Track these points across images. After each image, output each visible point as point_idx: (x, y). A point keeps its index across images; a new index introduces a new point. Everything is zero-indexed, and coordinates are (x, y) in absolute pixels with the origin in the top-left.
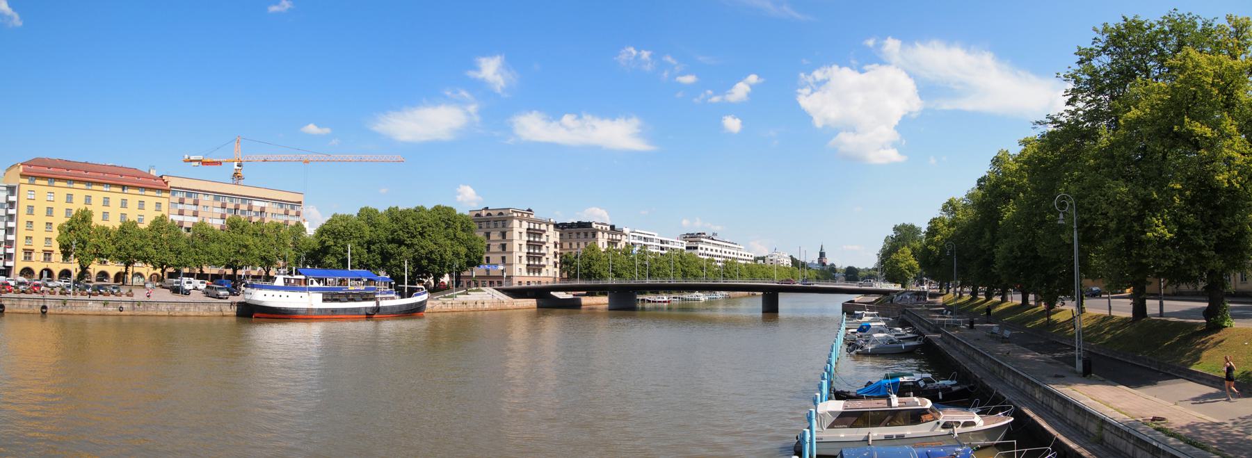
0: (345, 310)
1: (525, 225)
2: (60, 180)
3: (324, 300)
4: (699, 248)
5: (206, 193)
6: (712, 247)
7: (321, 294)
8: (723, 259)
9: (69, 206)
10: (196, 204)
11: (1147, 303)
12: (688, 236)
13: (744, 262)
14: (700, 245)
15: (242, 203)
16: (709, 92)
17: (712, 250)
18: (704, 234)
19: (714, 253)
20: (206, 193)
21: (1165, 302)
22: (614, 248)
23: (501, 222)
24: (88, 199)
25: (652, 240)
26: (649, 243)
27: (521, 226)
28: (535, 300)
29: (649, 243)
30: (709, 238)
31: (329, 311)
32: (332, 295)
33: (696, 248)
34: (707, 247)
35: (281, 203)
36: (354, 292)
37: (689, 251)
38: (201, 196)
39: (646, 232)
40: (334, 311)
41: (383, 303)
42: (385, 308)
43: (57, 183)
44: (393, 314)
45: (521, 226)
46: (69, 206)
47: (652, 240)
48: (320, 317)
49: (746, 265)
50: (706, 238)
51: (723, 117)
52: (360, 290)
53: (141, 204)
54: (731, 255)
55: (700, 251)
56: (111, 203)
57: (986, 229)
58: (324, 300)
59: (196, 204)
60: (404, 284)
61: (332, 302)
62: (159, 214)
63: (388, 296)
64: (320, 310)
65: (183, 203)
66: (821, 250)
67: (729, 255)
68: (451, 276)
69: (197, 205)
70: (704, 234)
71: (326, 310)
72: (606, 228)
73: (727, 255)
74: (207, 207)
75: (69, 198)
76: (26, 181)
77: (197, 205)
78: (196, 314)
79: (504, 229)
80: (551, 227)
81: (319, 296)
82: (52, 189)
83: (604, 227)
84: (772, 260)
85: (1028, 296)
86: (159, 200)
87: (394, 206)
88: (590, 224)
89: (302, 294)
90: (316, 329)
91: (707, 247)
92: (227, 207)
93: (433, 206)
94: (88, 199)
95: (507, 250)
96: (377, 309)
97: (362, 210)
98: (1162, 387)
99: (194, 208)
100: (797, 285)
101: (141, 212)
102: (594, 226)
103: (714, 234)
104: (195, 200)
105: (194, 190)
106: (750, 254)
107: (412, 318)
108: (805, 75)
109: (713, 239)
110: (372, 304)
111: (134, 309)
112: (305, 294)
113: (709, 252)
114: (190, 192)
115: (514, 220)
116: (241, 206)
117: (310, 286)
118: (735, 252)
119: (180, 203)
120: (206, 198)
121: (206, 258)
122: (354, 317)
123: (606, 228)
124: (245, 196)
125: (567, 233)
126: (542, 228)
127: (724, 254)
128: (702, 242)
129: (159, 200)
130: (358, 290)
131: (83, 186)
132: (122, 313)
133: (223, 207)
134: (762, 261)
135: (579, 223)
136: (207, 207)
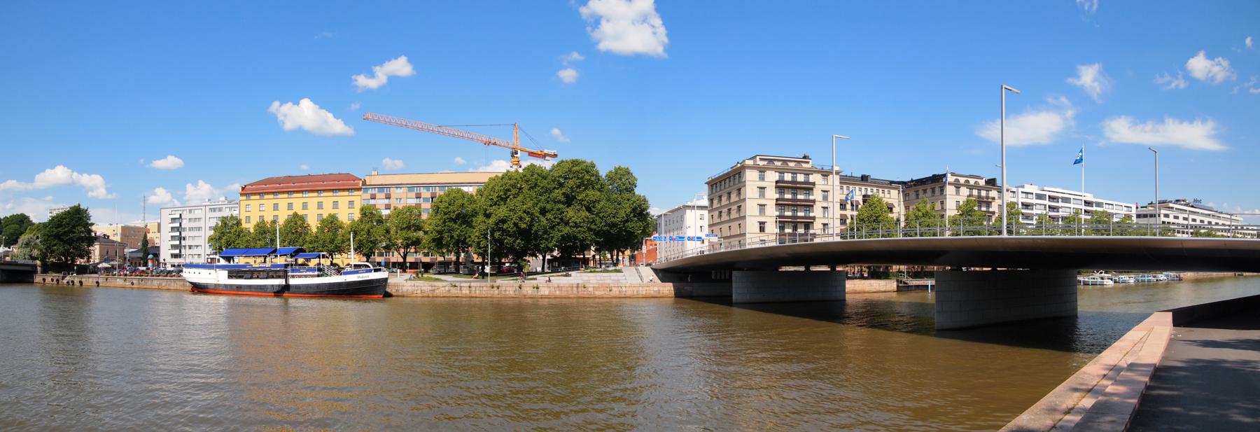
0: (250, 287)
1: (772, 176)
2: (268, 193)
3: (230, 277)
5: (398, 186)
7: (227, 272)
9: (320, 212)
10: (388, 197)
15: (379, 192)
20: (398, 186)
24: (335, 205)
28: (671, 284)
31: (235, 288)
32: (238, 272)
35: (411, 187)
36: (260, 269)
38: (393, 190)
40: (239, 287)
41: (292, 282)
42: (298, 287)
43: (266, 197)
44: (310, 294)
46: (320, 212)
48: (226, 292)
51: (354, 77)
52: (265, 267)
53: (276, 207)
56: (340, 205)
58: (230, 277)
59: (388, 197)
61: (237, 278)
62: (291, 213)
63: (308, 273)
64: (226, 285)
65: (375, 198)
69: (389, 198)
71: (231, 286)
74: (400, 199)
75: (320, 206)
76: (244, 198)
77: (389, 198)
78: (175, 288)
81: (226, 273)
82: (262, 202)
86: (351, 199)
89: (210, 271)
90: (222, 299)
92: (422, 196)
94: (335, 205)
96: (287, 287)
97: (618, 170)
99: (387, 201)
101: (276, 213)
104: (386, 194)
105: (386, 185)
107: (357, 301)
109: (1192, 206)
110: (281, 282)
111: (139, 283)
112: (212, 271)
114: (381, 187)
116: (377, 195)
117: (217, 264)
119: (372, 199)
120: (399, 191)
122: (260, 294)
124: (381, 185)
129: (351, 199)
130: (263, 267)
131: (286, 196)
132: (133, 286)
133: (418, 196)
135: (934, 176)
136: (400, 199)
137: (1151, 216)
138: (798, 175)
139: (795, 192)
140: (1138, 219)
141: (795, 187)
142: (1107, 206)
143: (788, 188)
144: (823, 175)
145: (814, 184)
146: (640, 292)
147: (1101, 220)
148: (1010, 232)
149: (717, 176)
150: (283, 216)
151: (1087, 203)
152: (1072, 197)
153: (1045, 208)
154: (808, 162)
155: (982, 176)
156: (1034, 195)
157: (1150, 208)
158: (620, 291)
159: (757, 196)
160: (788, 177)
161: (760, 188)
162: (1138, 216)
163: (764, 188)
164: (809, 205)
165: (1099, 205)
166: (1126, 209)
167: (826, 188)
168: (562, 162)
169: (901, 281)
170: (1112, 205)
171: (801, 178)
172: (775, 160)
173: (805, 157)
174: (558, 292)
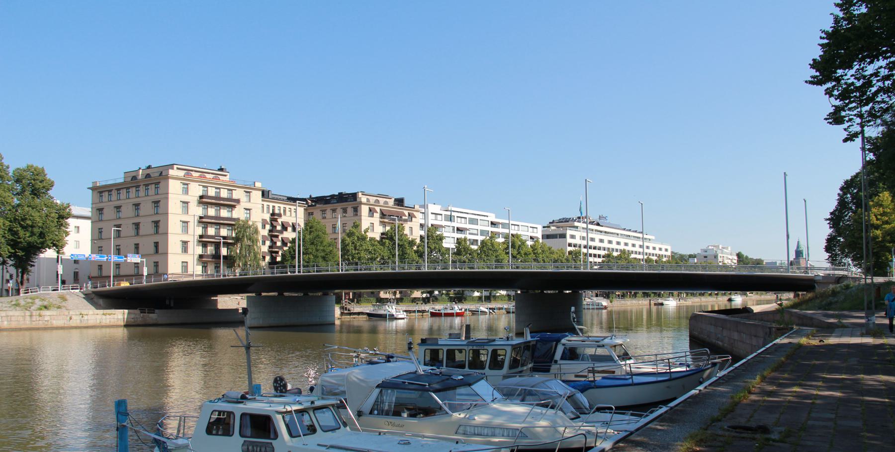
1: (196, 190)
4: (568, 236)
8: (602, 253)
14: (569, 232)
16: (853, 189)
17: (634, 245)
23: (153, 186)
27: (186, 191)
37: (549, 243)
45: (186, 191)
54: (657, 252)
55: (569, 240)
58: (61, 274)
67: (655, 252)
72: (386, 203)
73: (651, 251)
79: (156, 198)
80: (257, 195)
85: (168, 172)
87: (40, 167)
91: (634, 242)
95: (159, 252)
98: (482, 410)
100: (550, 270)
106: (664, 247)
109: (598, 224)
113: (606, 245)
115: (362, 206)
118: (651, 245)
121: (198, 358)
125: (318, 211)
126: (235, 197)
127: (646, 251)
128: (577, 227)
135: (340, 194)
137: (592, 316)
138: (209, 188)
139: (218, 208)
140: (564, 232)
141: (219, 203)
142: (459, 219)
143: (212, 204)
144: (246, 192)
145: (238, 201)
146: (104, 321)
147: (514, 244)
148: (342, 271)
149: (104, 183)
150: (463, 237)
151: (493, 224)
152: (479, 218)
153: (454, 230)
154: (225, 176)
156: (443, 216)
157: (553, 228)
158: (81, 321)
159: (152, 212)
160: (212, 192)
161: (184, 202)
162: (145, 310)
163: (187, 203)
164: (203, 221)
165: (504, 226)
166: (531, 230)
167: (248, 206)
168: (14, 171)
169: (346, 308)
170: (518, 225)
171: (224, 194)
172: (192, 171)
173: (221, 169)
174: (6, 323)
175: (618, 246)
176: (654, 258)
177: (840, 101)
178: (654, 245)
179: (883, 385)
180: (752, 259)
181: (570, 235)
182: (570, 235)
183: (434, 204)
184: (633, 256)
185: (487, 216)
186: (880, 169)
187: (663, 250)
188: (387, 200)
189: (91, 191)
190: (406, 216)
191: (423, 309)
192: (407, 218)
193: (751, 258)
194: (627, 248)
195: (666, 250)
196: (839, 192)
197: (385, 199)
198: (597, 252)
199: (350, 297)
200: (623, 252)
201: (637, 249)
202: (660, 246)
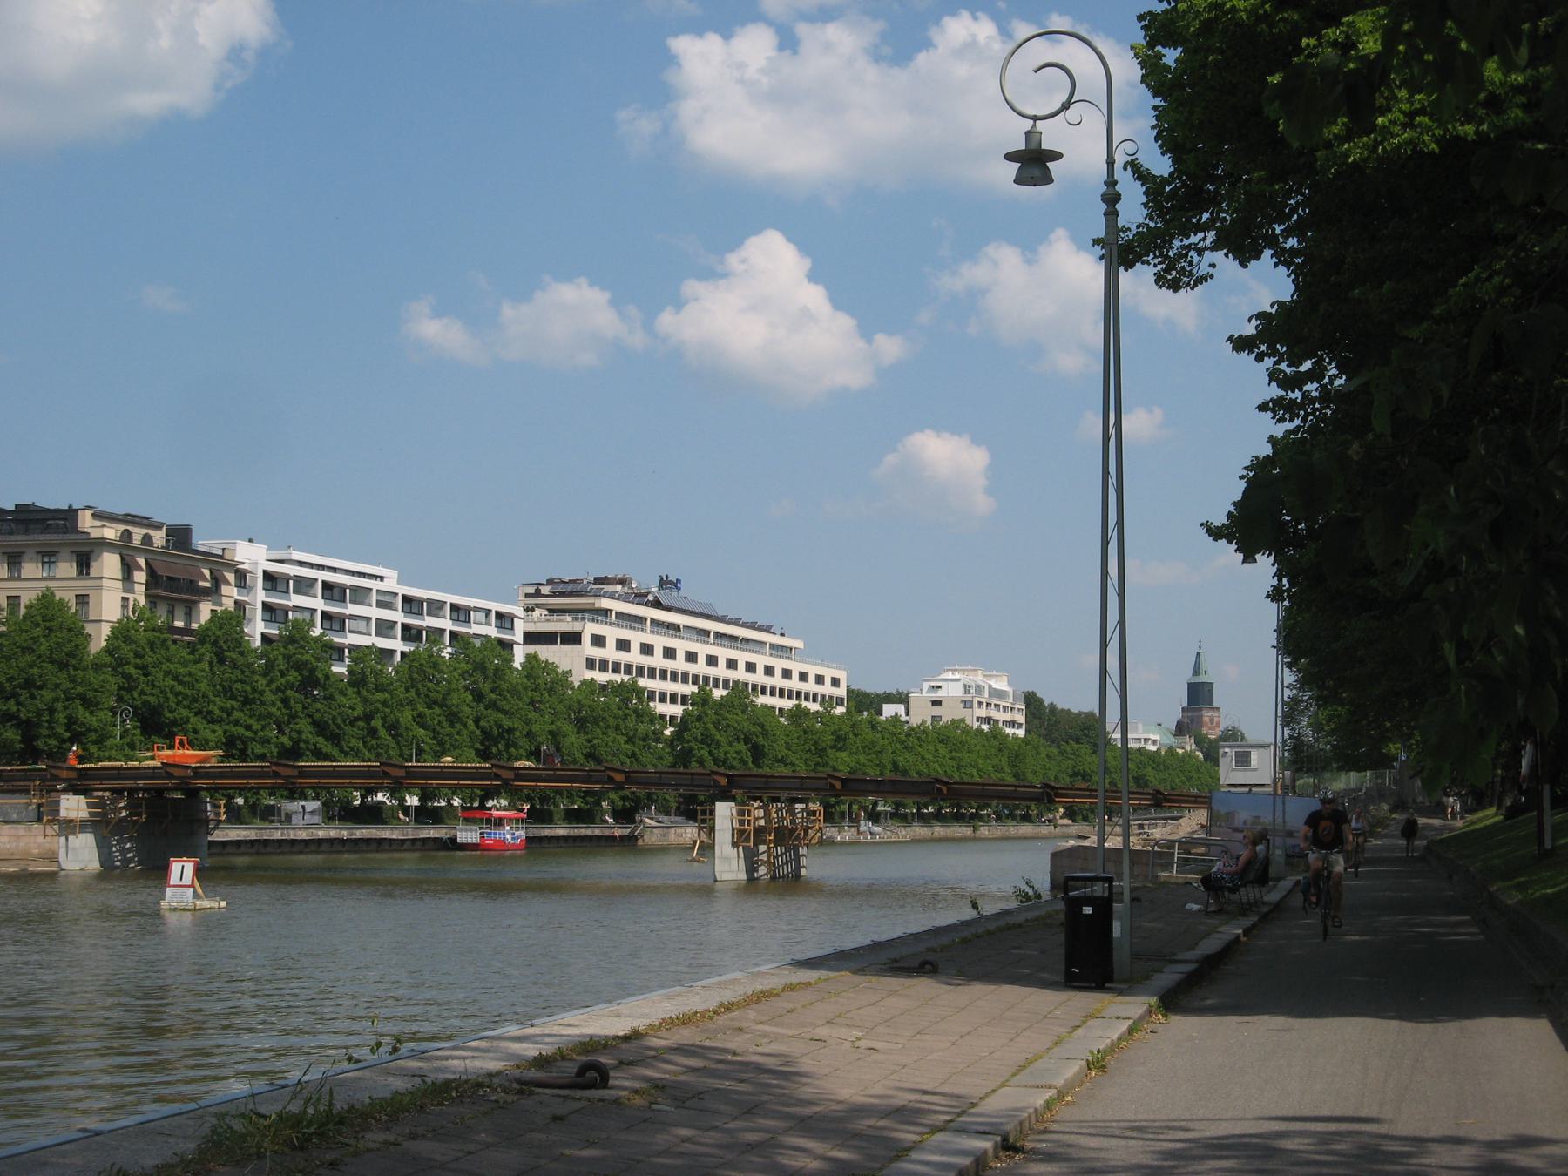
4: (586, 639)
6: (648, 638)
8: (689, 689)
11: (1114, 909)
12: (545, 590)
13: (788, 704)
18: (622, 582)
19: (634, 657)
21: (171, 883)
22: (179, 623)
25: (360, 595)
26: (352, 609)
29: (352, 609)
30: (640, 598)
33: (573, 638)
34: (626, 634)
39: (343, 567)
47: (360, 595)
49: (798, 715)
50: (625, 598)
57: (1425, 325)
60: (1174, 849)
66: (1196, 672)
68: (221, 800)
70: (622, 582)
72: (147, 539)
83: (138, 534)
84: (937, 703)
88: (71, 514)
91: (626, 634)
93: (1066, 708)
102: (86, 522)
103: (664, 583)
106: (829, 674)
108: (1367, 136)
109: (657, 604)
123: (147, 539)
134: (900, 709)
135: (22, 509)
155: (157, 518)
175: (833, 688)
176: (814, 707)
177: (1164, 56)
178: (805, 668)
179: (1341, 1163)
180: (1069, 712)
181: (592, 635)
182: (592, 635)
183: (250, 541)
184: (762, 700)
185: (382, 578)
186: (1277, 215)
187: (702, 659)
188: (152, 532)
189: (893, 714)
190: (205, 579)
191: (292, 837)
192: (207, 585)
193: (1063, 710)
194: (750, 678)
195: (835, 682)
196: (1232, 509)
197: (144, 531)
198: (669, 687)
199: (1552, 790)
200: (738, 689)
201: (777, 681)
202: (821, 671)
